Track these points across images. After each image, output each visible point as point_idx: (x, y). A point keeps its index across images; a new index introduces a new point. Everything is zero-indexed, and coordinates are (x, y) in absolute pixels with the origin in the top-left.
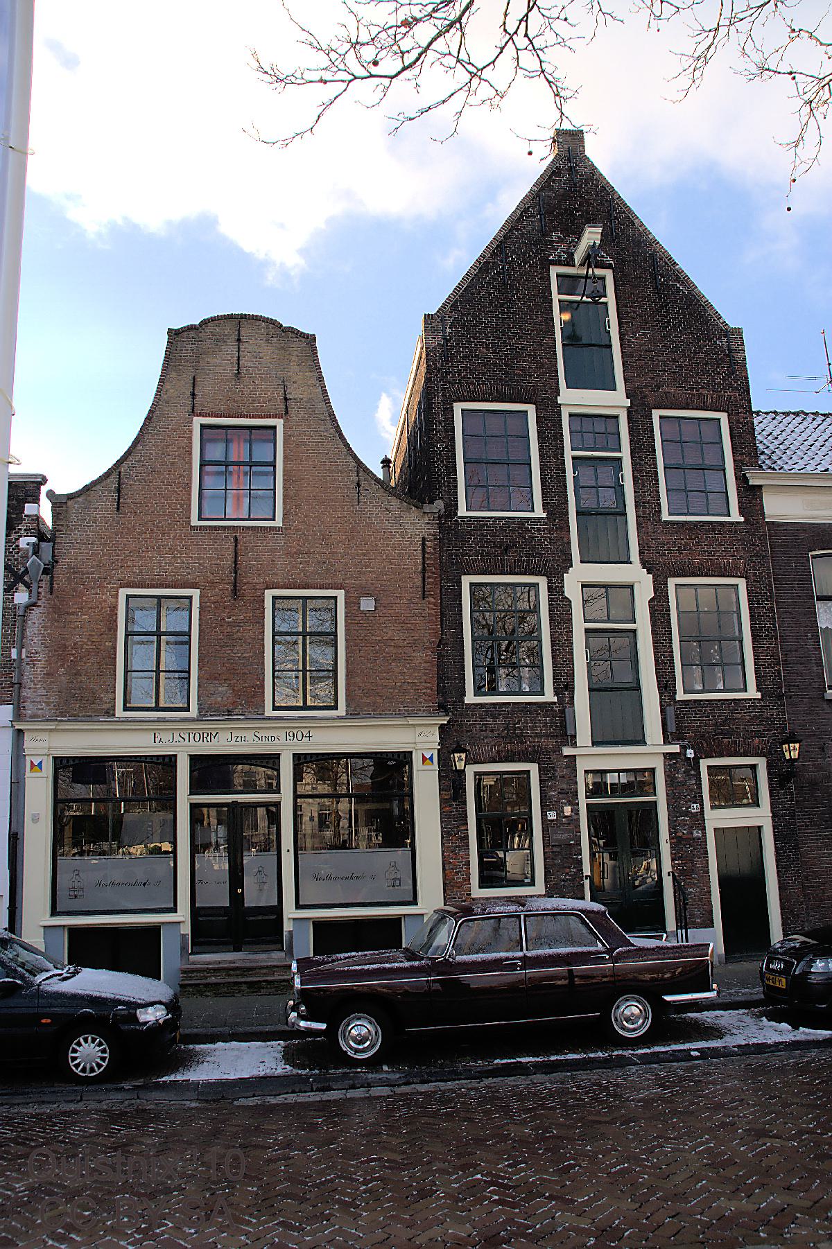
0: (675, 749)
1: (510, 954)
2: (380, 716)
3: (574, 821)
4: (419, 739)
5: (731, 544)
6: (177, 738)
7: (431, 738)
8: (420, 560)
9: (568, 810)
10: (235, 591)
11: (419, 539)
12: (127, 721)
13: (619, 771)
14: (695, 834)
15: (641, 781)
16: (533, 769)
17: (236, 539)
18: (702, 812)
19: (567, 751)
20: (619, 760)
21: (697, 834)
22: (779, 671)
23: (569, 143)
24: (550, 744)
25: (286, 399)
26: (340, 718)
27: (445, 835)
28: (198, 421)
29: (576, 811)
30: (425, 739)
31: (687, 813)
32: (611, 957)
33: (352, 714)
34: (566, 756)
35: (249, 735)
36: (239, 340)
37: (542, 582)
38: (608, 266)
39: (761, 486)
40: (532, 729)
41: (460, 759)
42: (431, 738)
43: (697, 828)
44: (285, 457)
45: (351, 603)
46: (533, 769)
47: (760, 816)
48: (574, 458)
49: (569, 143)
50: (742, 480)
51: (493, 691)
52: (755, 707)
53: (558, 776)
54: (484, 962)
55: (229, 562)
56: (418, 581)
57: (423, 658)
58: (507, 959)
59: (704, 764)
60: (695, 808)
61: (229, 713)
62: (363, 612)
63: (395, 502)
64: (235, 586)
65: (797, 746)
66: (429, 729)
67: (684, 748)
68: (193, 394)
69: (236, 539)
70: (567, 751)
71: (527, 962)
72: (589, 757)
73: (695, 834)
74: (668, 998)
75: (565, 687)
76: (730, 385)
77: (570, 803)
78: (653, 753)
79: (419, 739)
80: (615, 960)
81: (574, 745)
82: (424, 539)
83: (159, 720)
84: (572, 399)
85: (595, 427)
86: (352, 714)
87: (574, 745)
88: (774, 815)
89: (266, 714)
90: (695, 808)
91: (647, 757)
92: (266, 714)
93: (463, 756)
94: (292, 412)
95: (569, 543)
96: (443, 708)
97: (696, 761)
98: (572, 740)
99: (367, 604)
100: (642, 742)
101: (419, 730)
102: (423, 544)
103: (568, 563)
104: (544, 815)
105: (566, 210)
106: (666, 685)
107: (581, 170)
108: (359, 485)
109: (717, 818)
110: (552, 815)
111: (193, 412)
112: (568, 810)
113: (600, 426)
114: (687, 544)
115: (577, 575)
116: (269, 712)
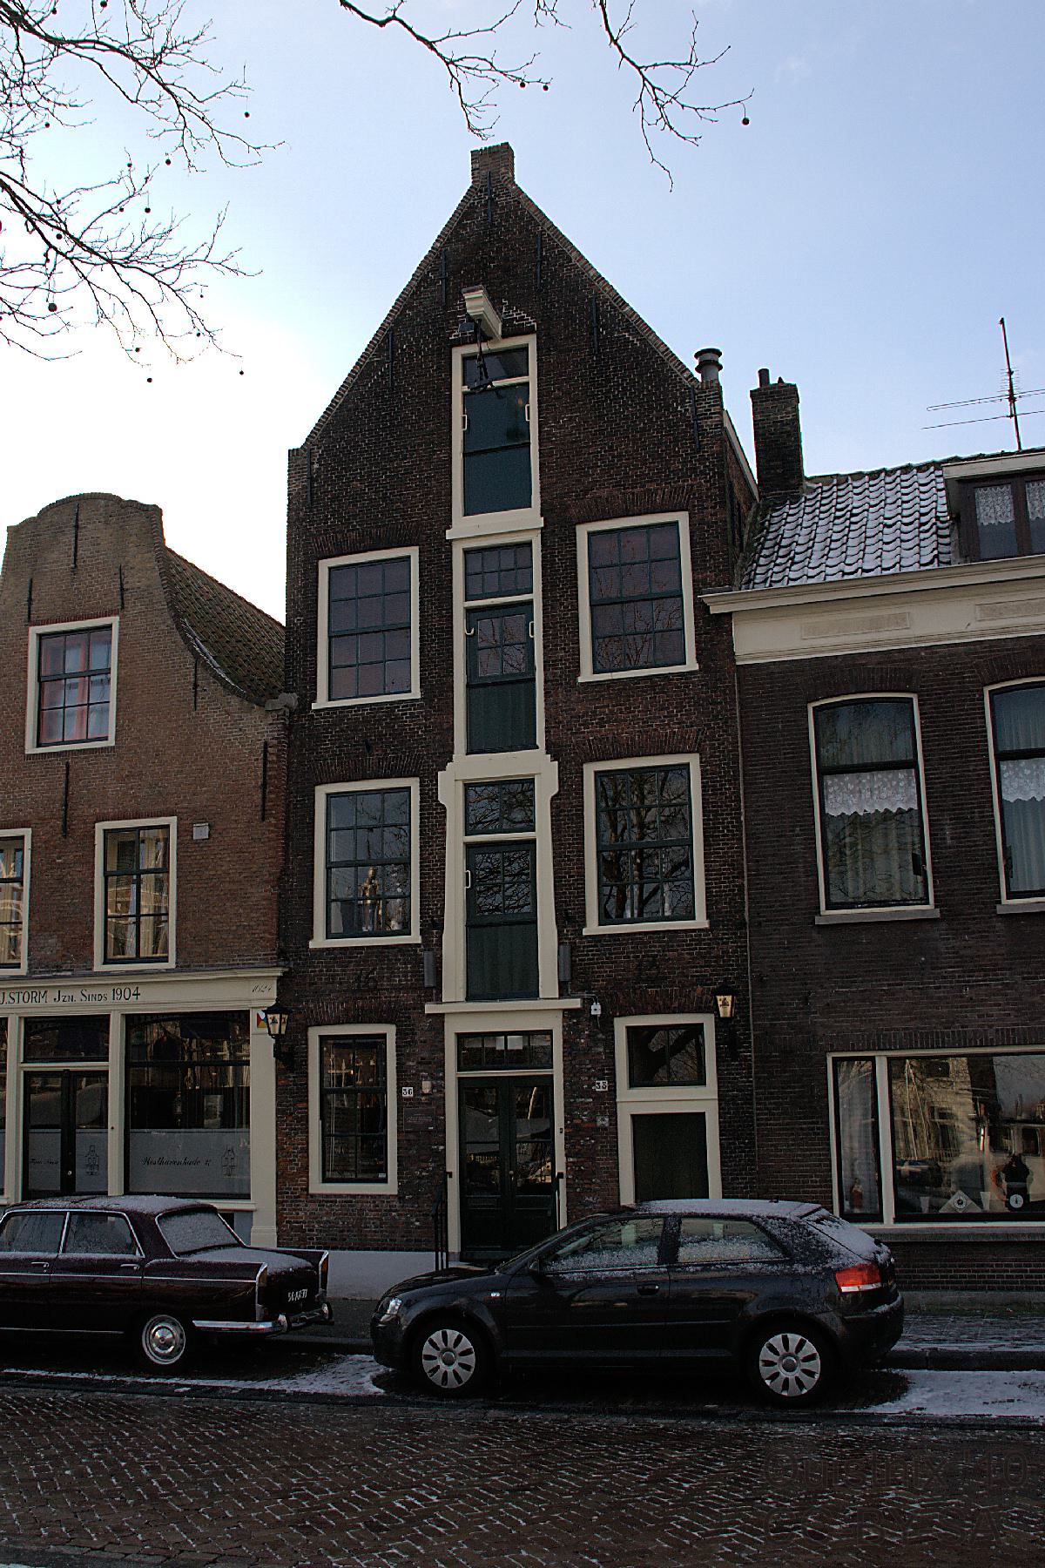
0: (575, 1003)
1: (37, 1254)
2: (214, 967)
3: (438, 1101)
4: (251, 992)
5: (680, 707)
6: (8, 999)
7: (266, 994)
8: (260, 773)
9: (426, 1086)
10: (65, 827)
11: (260, 745)
12: (108, 974)
13: (506, 1034)
14: (599, 1123)
15: (533, 1051)
16: (390, 1031)
17: (68, 765)
18: (613, 1089)
19: (430, 1008)
20: (504, 1018)
21: (603, 1122)
22: (741, 887)
23: (493, 164)
24: (407, 998)
25: (122, 589)
26: (168, 971)
27: (281, 1112)
28: (34, 631)
29: (439, 1088)
30: (262, 995)
31: (590, 1093)
32: (142, 1266)
33: (182, 967)
34: (429, 1015)
35: (77, 994)
36: (77, 527)
37: (414, 784)
38: (530, 331)
39: (730, 614)
40: (389, 979)
41: (725, 1004)
42: (266, 994)
43: (603, 1114)
44: (119, 661)
45: (184, 831)
46: (390, 1031)
47: (702, 1100)
48: (468, 611)
49: (493, 164)
50: (701, 608)
51: (621, 919)
52: (700, 941)
53: (422, 1041)
54: (15, 1260)
55: (60, 795)
56: (258, 797)
57: (261, 893)
58: (124, 1261)
59: (621, 1025)
60: (601, 1086)
61: (59, 968)
62: (197, 842)
63: (235, 701)
64: (65, 822)
65: (729, 998)
66: (262, 983)
67: (588, 1003)
68: (30, 600)
69: (68, 765)
70: (430, 1008)
71: (55, 1265)
72: (459, 1012)
73: (599, 1123)
74: (197, 1323)
75: (433, 924)
76: (694, 469)
77: (432, 1077)
78: (544, 1011)
79: (256, 995)
80: (149, 1272)
81: (439, 1000)
82: (266, 744)
83: (128, 973)
84: (468, 529)
85: (497, 562)
86: (182, 967)
87: (439, 1000)
88: (721, 1098)
89: (95, 969)
90: (601, 1086)
91: (467, 1018)
92: (95, 969)
93: (729, 998)
94: (128, 605)
95: (451, 728)
96: (282, 955)
97: (606, 1024)
98: (435, 993)
99: (201, 832)
100: (535, 995)
101: (253, 984)
102: (265, 752)
103: (448, 756)
104: (399, 1092)
105: (477, 263)
106: (570, 916)
107: (501, 200)
108: (196, 686)
109: (635, 1101)
110: (408, 1092)
111: (31, 622)
112: (426, 1086)
113: (507, 560)
114: (611, 712)
115: (465, 767)
116: (98, 966)
